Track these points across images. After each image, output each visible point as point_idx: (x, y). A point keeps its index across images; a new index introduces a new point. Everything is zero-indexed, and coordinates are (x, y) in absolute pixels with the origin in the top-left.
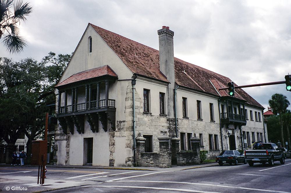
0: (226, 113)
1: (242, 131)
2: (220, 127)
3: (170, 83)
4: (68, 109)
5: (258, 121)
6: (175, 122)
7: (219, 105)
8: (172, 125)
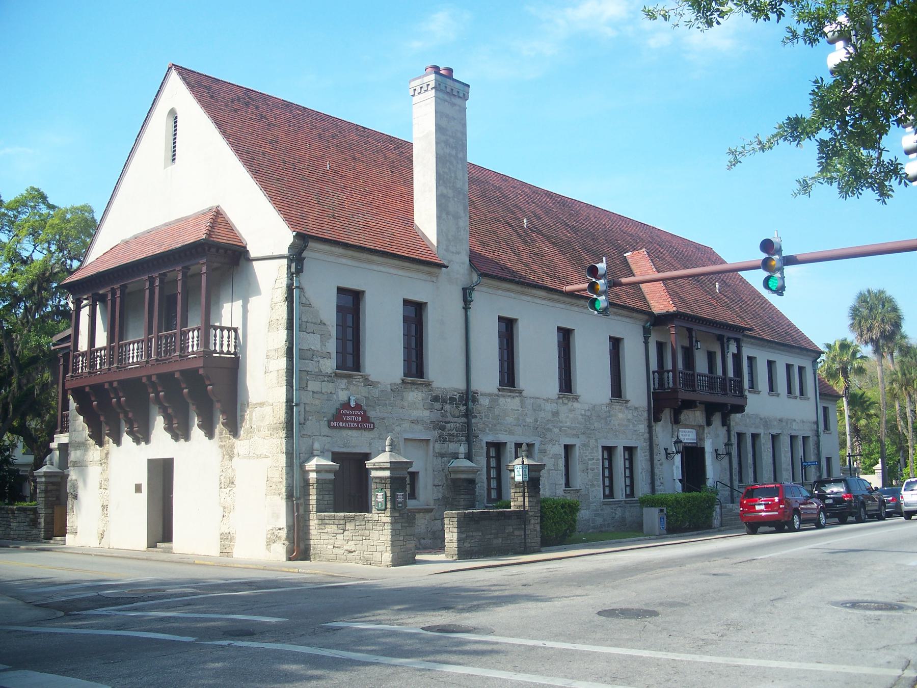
0: (668, 372)
1: (732, 433)
2: (649, 420)
3: (447, 267)
4: (190, 344)
5: (796, 398)
6: (466, 404)
7: (646, 343)
8: (454, 416)
